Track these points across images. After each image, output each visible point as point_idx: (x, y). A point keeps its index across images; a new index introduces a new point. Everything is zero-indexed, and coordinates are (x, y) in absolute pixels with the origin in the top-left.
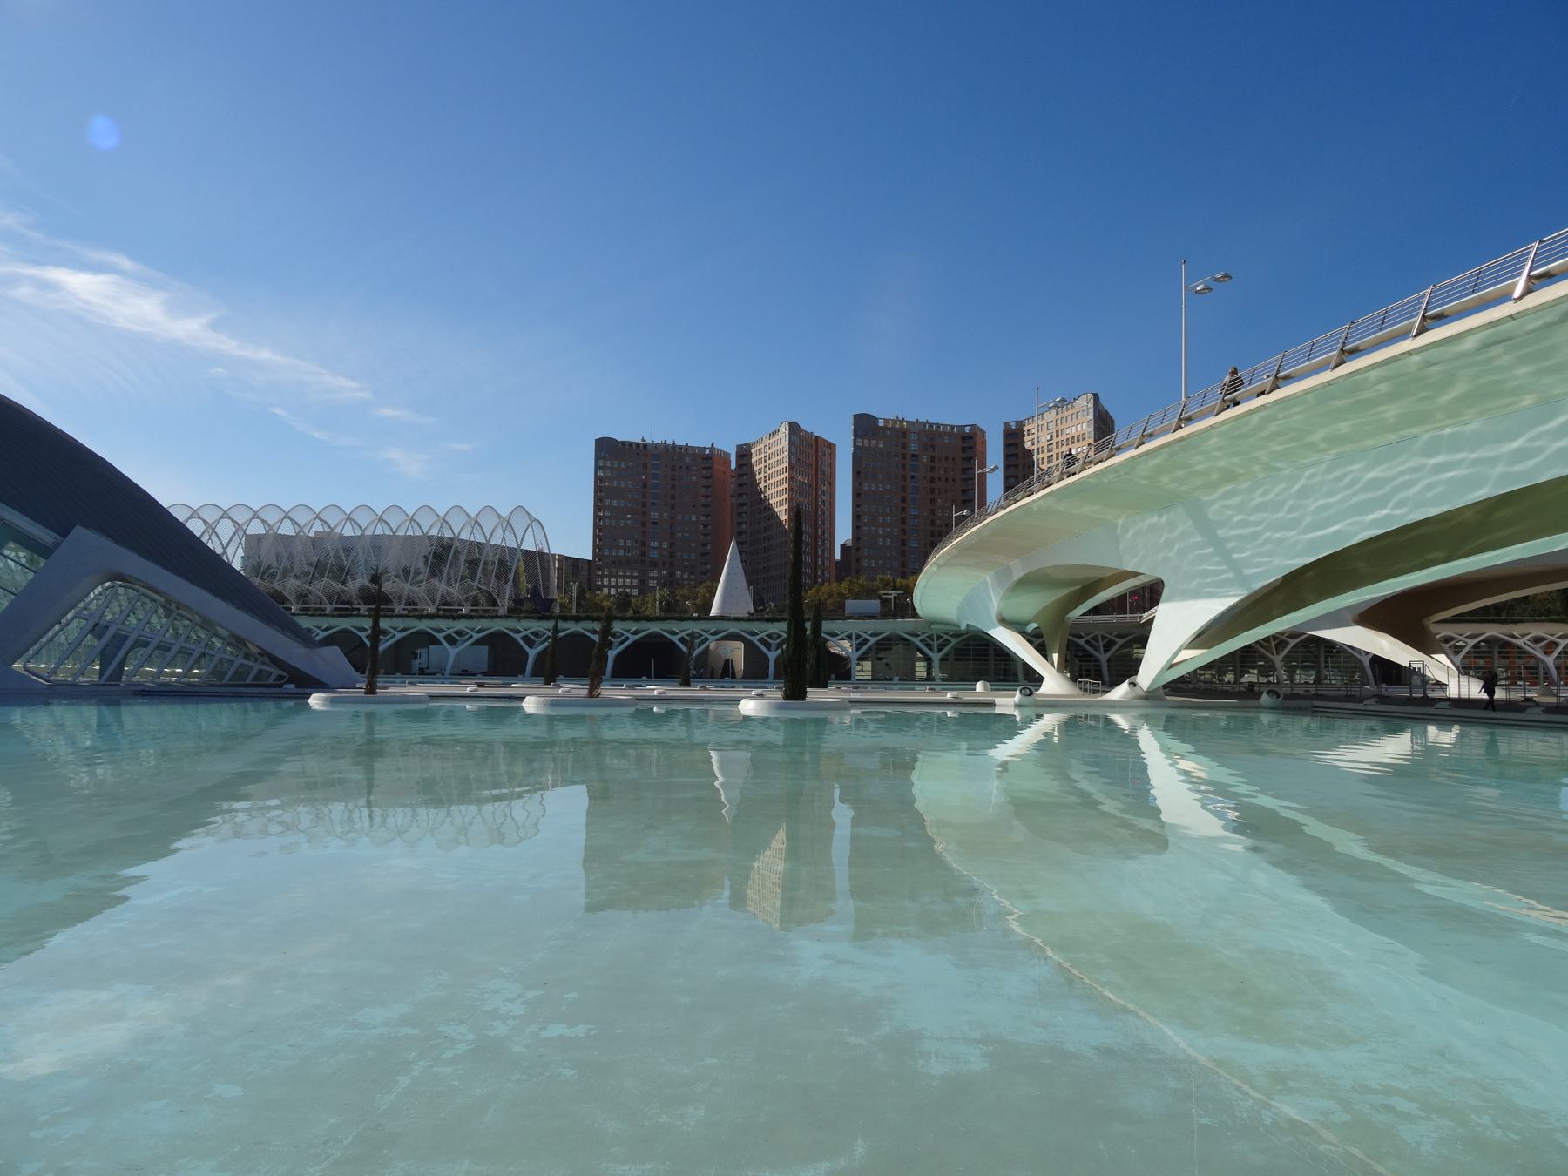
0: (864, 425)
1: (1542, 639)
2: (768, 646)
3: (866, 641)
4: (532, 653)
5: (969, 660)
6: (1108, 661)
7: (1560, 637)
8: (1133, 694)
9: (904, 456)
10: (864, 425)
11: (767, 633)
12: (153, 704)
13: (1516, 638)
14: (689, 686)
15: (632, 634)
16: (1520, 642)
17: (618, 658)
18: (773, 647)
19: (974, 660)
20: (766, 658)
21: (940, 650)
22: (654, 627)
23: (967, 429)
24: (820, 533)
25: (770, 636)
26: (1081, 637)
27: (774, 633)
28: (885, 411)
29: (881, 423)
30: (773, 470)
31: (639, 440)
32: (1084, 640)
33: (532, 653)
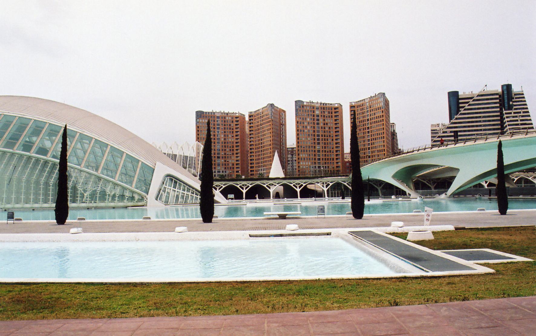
0: (299, 105)
1: (299, 184)
2: (243, 189)
3: (248, 186)
4: (244, 191)
5: (387, 189)
6: (327, 190)
7: (304, 183)
8: (446, 197)
9: (314, 116)
10: (299, 105)
11: (269, 184)
12: (481, 202)
13: (529, 177)
14: (344, 199)
15: (223, 185)
16: (530, 178)
17: (246, 193)
18: (244, 189)
19: (389, 189)
20: (242, 193)
21: (326, 187)
22: (258, 182)
23: (336, 105)
24: (282, 148)
25: (243, 185)
26: (265, 184)
27: (245, 184)
28: (306, 99)
29: (305, 104)
30: (264, 122)
31: (211, 111)
32: (239, 186)
33: (244, 191)
